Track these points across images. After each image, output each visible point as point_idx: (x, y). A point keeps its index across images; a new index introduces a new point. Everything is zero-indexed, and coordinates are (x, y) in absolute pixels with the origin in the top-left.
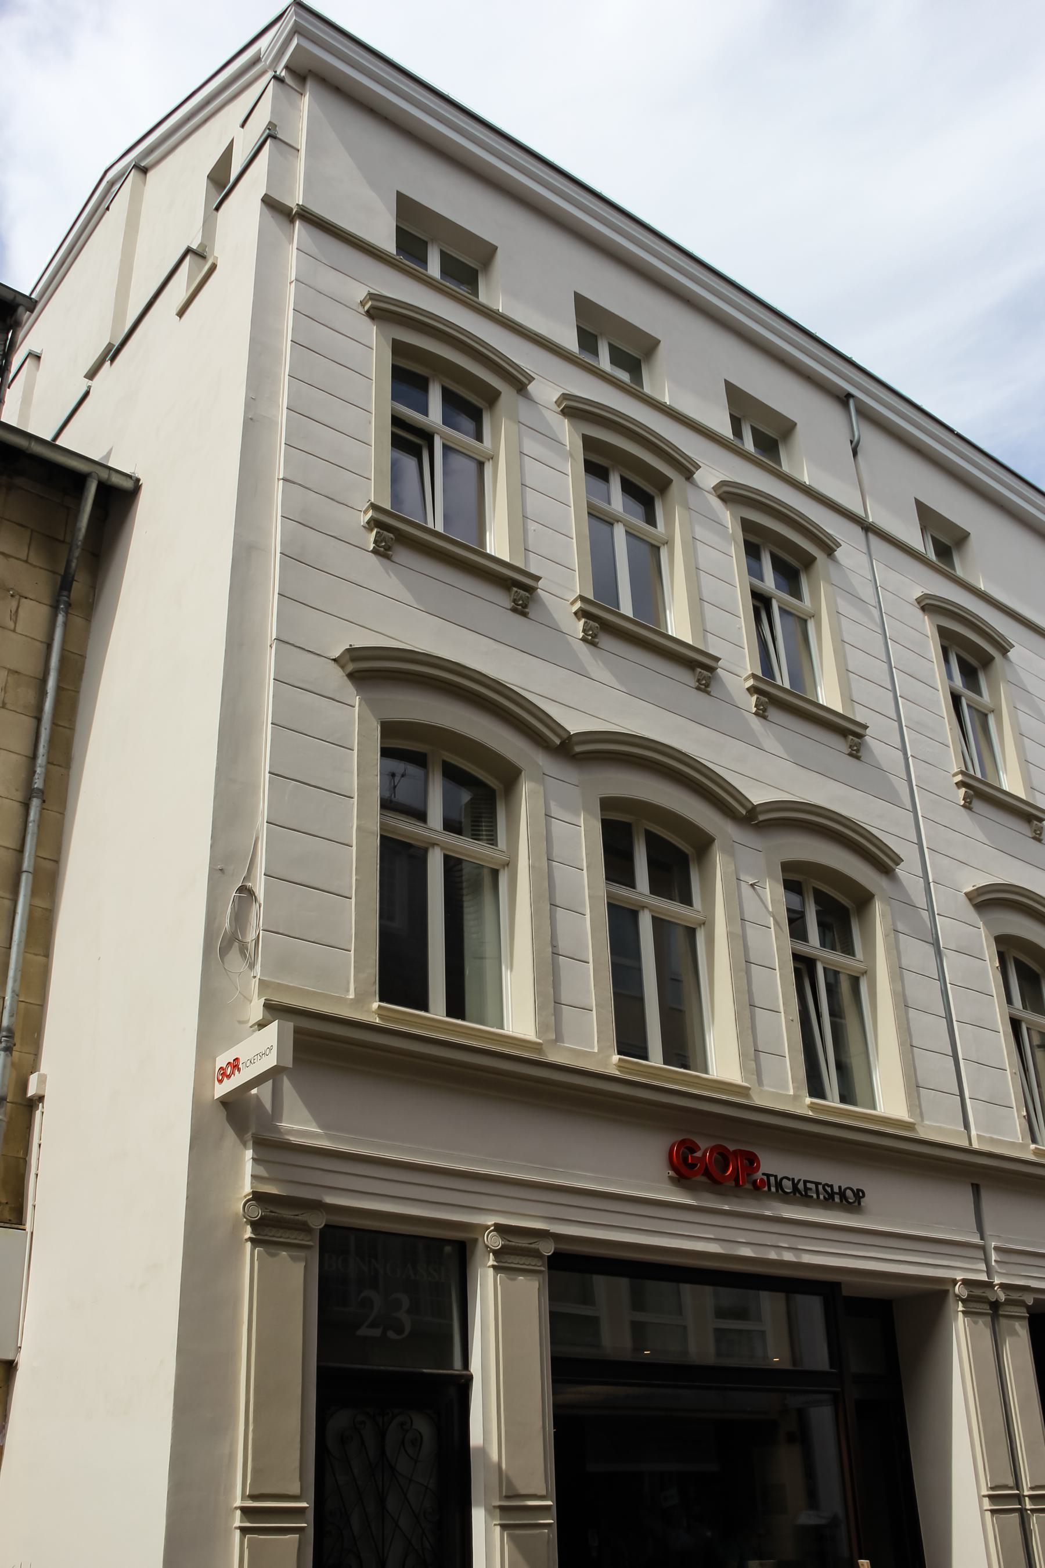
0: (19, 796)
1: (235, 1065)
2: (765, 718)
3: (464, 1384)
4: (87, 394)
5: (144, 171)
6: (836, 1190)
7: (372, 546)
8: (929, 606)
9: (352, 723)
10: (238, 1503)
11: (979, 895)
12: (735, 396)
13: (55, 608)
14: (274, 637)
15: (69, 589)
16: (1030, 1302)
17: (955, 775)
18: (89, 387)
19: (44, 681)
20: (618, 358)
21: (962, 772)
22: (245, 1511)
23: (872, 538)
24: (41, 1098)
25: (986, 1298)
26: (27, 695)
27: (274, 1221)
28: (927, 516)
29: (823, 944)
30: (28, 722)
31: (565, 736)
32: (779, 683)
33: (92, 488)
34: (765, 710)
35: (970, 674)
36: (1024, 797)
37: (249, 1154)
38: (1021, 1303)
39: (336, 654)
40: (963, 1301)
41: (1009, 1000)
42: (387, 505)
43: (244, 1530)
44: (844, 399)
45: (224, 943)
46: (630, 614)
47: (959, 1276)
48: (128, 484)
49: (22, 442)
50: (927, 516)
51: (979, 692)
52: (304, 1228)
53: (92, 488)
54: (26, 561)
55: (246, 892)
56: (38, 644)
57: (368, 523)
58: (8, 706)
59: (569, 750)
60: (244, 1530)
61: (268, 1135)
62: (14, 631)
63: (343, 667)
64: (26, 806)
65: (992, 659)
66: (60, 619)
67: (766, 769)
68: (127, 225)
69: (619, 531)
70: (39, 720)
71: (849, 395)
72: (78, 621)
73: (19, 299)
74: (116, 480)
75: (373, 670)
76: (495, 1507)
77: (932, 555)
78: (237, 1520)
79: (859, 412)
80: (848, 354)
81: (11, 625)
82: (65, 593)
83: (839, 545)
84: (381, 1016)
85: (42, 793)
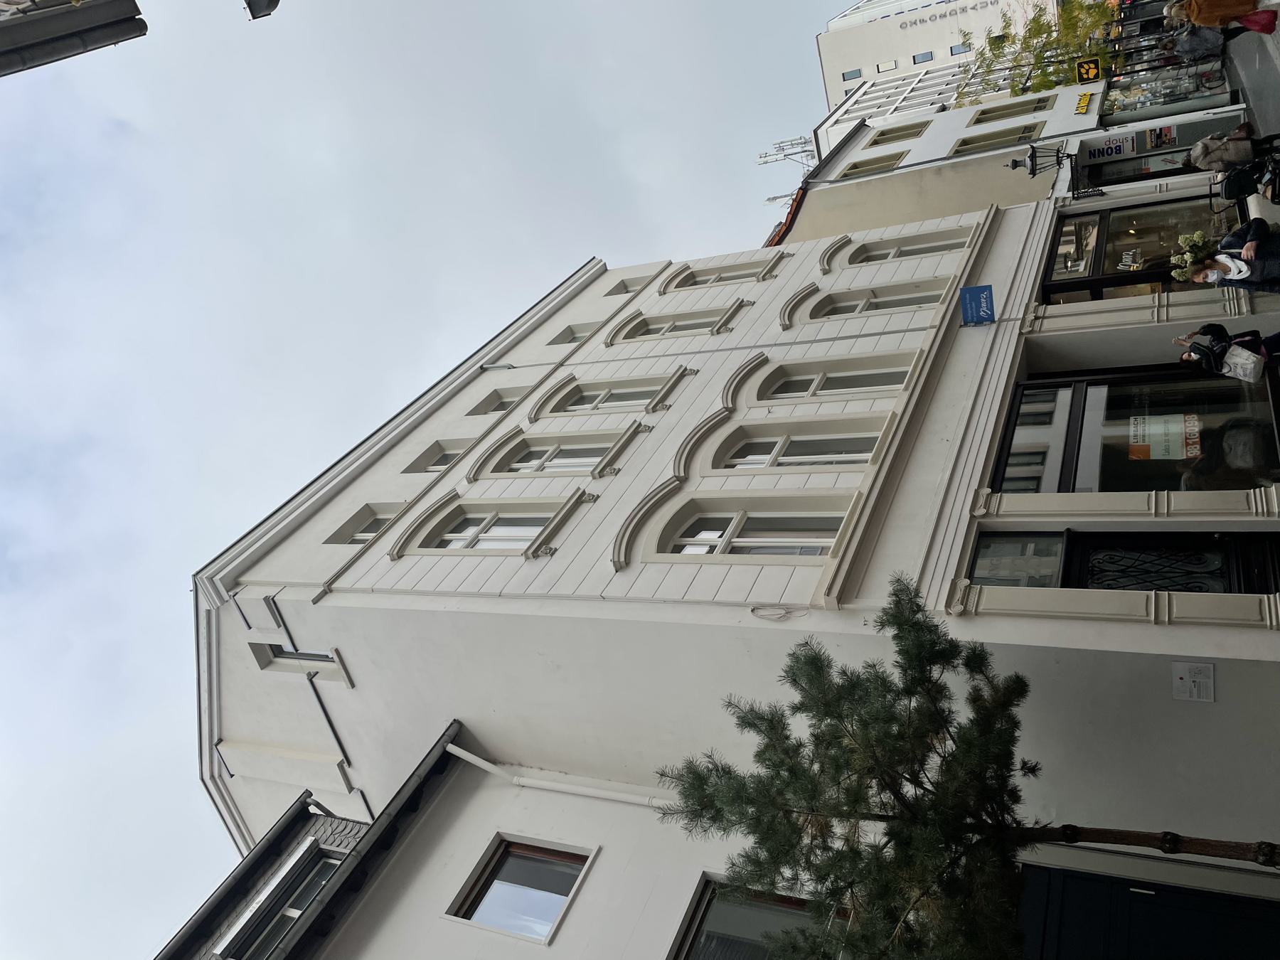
33: (452, 748)
44: (483, 369)
67: (650, 466)
71: (481, 367)
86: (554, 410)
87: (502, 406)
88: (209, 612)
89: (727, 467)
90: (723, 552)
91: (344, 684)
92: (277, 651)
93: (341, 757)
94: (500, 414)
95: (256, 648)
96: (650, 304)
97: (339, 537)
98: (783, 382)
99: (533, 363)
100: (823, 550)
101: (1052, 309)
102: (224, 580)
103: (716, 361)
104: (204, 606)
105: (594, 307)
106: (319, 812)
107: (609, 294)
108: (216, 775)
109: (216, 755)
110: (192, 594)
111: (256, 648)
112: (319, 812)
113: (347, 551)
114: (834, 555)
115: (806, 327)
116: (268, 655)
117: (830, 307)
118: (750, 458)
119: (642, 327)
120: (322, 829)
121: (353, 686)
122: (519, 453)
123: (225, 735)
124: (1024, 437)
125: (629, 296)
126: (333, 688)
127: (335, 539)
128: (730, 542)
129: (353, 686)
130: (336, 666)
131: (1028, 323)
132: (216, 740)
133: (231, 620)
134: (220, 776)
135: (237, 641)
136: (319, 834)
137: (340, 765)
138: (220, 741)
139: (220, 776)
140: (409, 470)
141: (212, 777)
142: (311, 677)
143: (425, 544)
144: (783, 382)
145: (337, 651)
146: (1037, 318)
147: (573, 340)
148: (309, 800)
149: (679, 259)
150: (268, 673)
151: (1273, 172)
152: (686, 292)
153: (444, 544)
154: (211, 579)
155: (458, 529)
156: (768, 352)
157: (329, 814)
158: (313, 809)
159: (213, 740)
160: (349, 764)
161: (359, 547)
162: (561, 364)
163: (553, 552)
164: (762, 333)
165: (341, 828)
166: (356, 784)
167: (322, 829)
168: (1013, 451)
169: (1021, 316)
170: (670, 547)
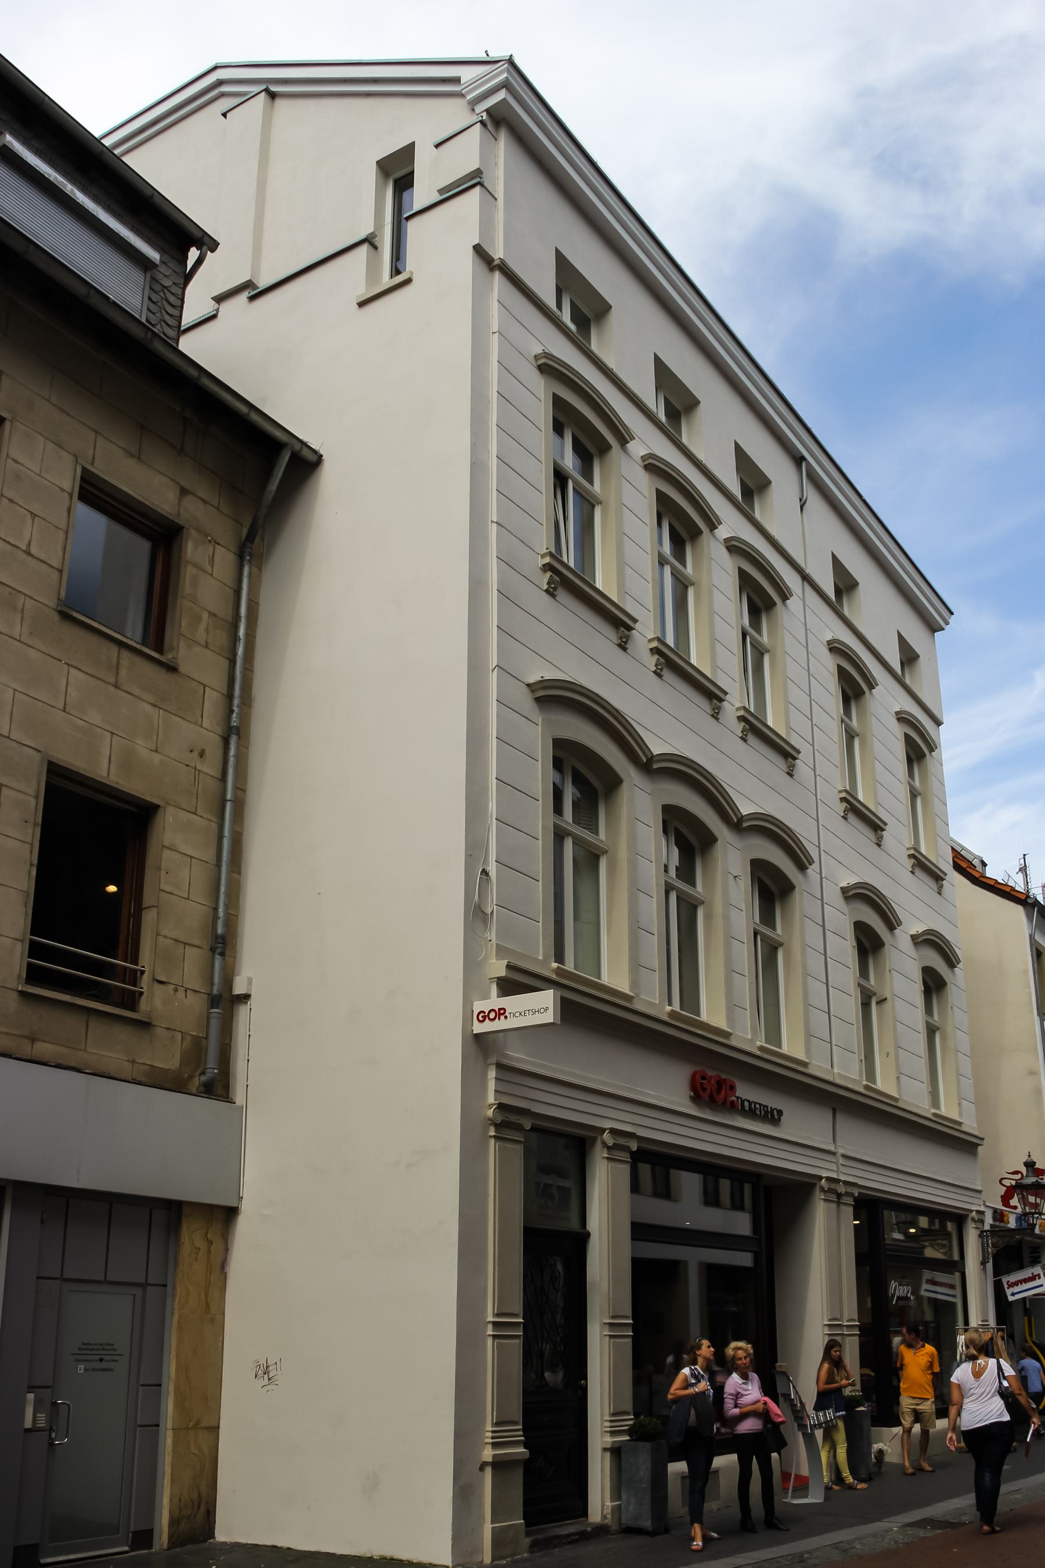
0: (219, 730)
1: (501, 1013)
2: (553, 596)
3: (582, 1238)
4: (213, 317)
5: (273, 96)
6: (1024, 1170)
7: (545, 587)
8: (549, 368)
9: (536, 734)
10: (490, 1318)
11: (543, 688)
12: (563, 265)
13: (241, 557)
14: (495, 664)
15: (252, 542)
16: (634, 1148)
17: (650, 641)
18: (218, 310)
19: (236, 628)
20: (577, 316)
21: (658, 639)
22: (495, 1324)
23: (806, 585)
24: (246, 997)
25: (628, 1147)
26: (221, 638)
27: (508, 1121)
28: (663, 374)
29: (576, 820)
30: (224, 663)
31: (650, 756)
32: (565, 559)
33: (285, 458)
34: (555, 589)
35: (678, 543)
36: (615, 599)
37: (492, 1074)
38: (626, 1149)
39: (531, 681)
40: (609, 1148)
41: (558, 809)
42: (554, 551)
43: (494, 1337)
44: (798, 460)
45: (476, 915)
46: (672, 645)
47: (608, 1125)
48: (313, 458)
49: (228, 397)
50: (663, 374)
51: (683, 563)
52: (519, 1128)
53: (285, 458)
54: (218, 509)
55: (485, 872)
56: (228, 590)
57: (544, 565)
58: (210, 646)
59: (651, 767)
60: (494, 1337)
61: (505, 1061)
62: (211, 575)
63: (533, 691)
64: (226, 742)
65: (773, 604)
66: (246, 570)
67: (666, 724)
68: (260, 155)
69: (667, 570)
70: (232, 662)
71: (803, 458)
72: (255, 570)
73: (206, 239)
74: (306, 453)
75: (555, 697)
76: (605, 1324)
77: (662, 417)
78: (490, 1331)
79: (809, 476)
80: (810, 425)
81: (209, 569)
82: (249, 545)
83: (720, 523)
84: (557, 974)
85: (237, 728)
86: (742, 573)
87: (748, 493)
88: (456, 80)
89: (665, 823)
90: (556, 826)
91: (364, 293)
92: (404, 184)
93: (263, 283)
94: (736, 490)
95: (407, 153)
96: (886, 699)
97: (567, 274)
98: (772, 890)
99: (801, 531)
100: (560, 957)
101: (848, 1211)
102: (517, 116)
103: (805, 805)
104: (467, 74)
105: (880, 614)
106: (190, 264)
107: (901, 639)
108: (224, 89)
109: (256, 89)
110: (482, 56)
111: (407, 153)
112: (190, 264)
113: (546, 290)
114: (559, 972)
115: (841, 919)
116: (398, 172)
117: (868, 945)
118: (676, 852)
119: (853, 688)
120: (168, 272)
121: (362, 304)
122: (681, 523)
123: (279, 102)
124: (690, 1183)
125: (898, 668)
126: (353, 274)
127: (563, 265)
128: (569, 834)
129: (362, 304)
130: (386, 280)
131: (833, 1186)
132: (273, 88)
133: (454, 114)
134: (223, 95)
135: (418, 124)
136: (163, 269)
137: (248, 285)
138: (273, 96)
139: (223, 95)
140: (660, 366)
141: (220, 83)
142: (370, 241)
143: (558, 403)
144: (772, 890)
145: (408, 281)
146: (839, 1196)
147: (838, 592)
148: (205, 248)
149: (945, 736)
150: (371, 172)
151: (851, 1487)
152: (899, 749)
153: (558, 428)
154: (505, 85)
155: (579, 449)
156: (812, 871)
157: (188, 277)
158: (193, 254)
159: (277, 87)
160: (252, 298)
161: (551, 302)
162: (805, 578)
163: (551, 593)
164: (841, 858)
165: (172, 299)
166: (226, 307)
167: (168, 272)
168: (672, 1171)
169: (843, 1178)
170: (560, 755)
